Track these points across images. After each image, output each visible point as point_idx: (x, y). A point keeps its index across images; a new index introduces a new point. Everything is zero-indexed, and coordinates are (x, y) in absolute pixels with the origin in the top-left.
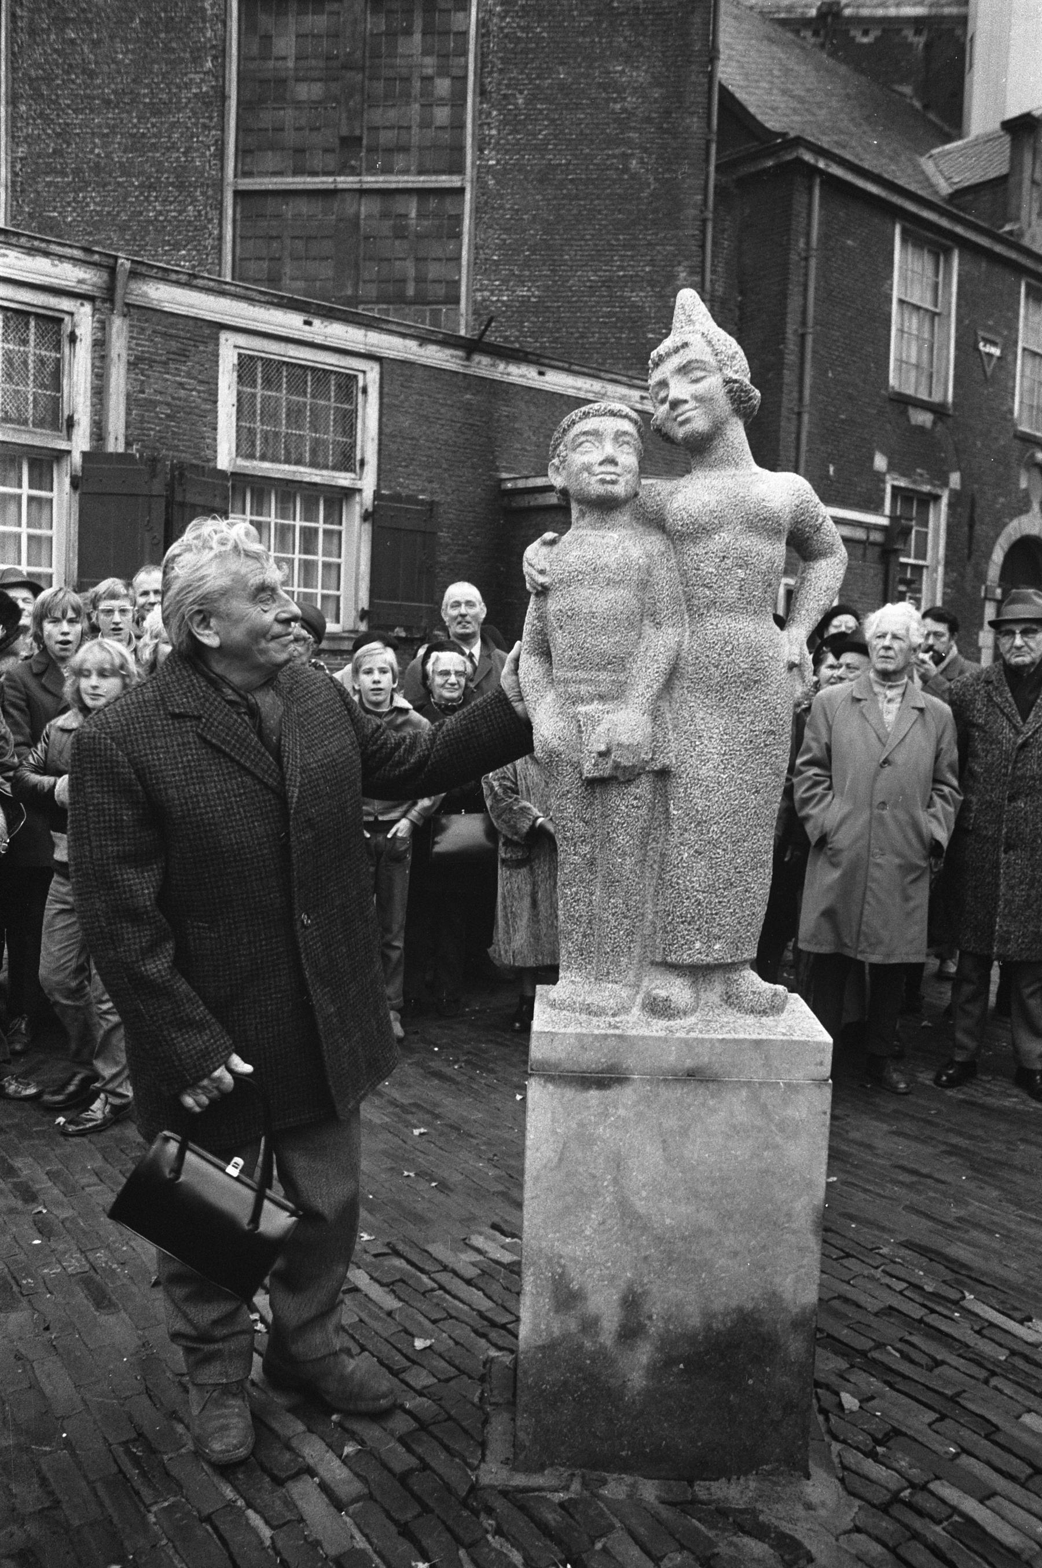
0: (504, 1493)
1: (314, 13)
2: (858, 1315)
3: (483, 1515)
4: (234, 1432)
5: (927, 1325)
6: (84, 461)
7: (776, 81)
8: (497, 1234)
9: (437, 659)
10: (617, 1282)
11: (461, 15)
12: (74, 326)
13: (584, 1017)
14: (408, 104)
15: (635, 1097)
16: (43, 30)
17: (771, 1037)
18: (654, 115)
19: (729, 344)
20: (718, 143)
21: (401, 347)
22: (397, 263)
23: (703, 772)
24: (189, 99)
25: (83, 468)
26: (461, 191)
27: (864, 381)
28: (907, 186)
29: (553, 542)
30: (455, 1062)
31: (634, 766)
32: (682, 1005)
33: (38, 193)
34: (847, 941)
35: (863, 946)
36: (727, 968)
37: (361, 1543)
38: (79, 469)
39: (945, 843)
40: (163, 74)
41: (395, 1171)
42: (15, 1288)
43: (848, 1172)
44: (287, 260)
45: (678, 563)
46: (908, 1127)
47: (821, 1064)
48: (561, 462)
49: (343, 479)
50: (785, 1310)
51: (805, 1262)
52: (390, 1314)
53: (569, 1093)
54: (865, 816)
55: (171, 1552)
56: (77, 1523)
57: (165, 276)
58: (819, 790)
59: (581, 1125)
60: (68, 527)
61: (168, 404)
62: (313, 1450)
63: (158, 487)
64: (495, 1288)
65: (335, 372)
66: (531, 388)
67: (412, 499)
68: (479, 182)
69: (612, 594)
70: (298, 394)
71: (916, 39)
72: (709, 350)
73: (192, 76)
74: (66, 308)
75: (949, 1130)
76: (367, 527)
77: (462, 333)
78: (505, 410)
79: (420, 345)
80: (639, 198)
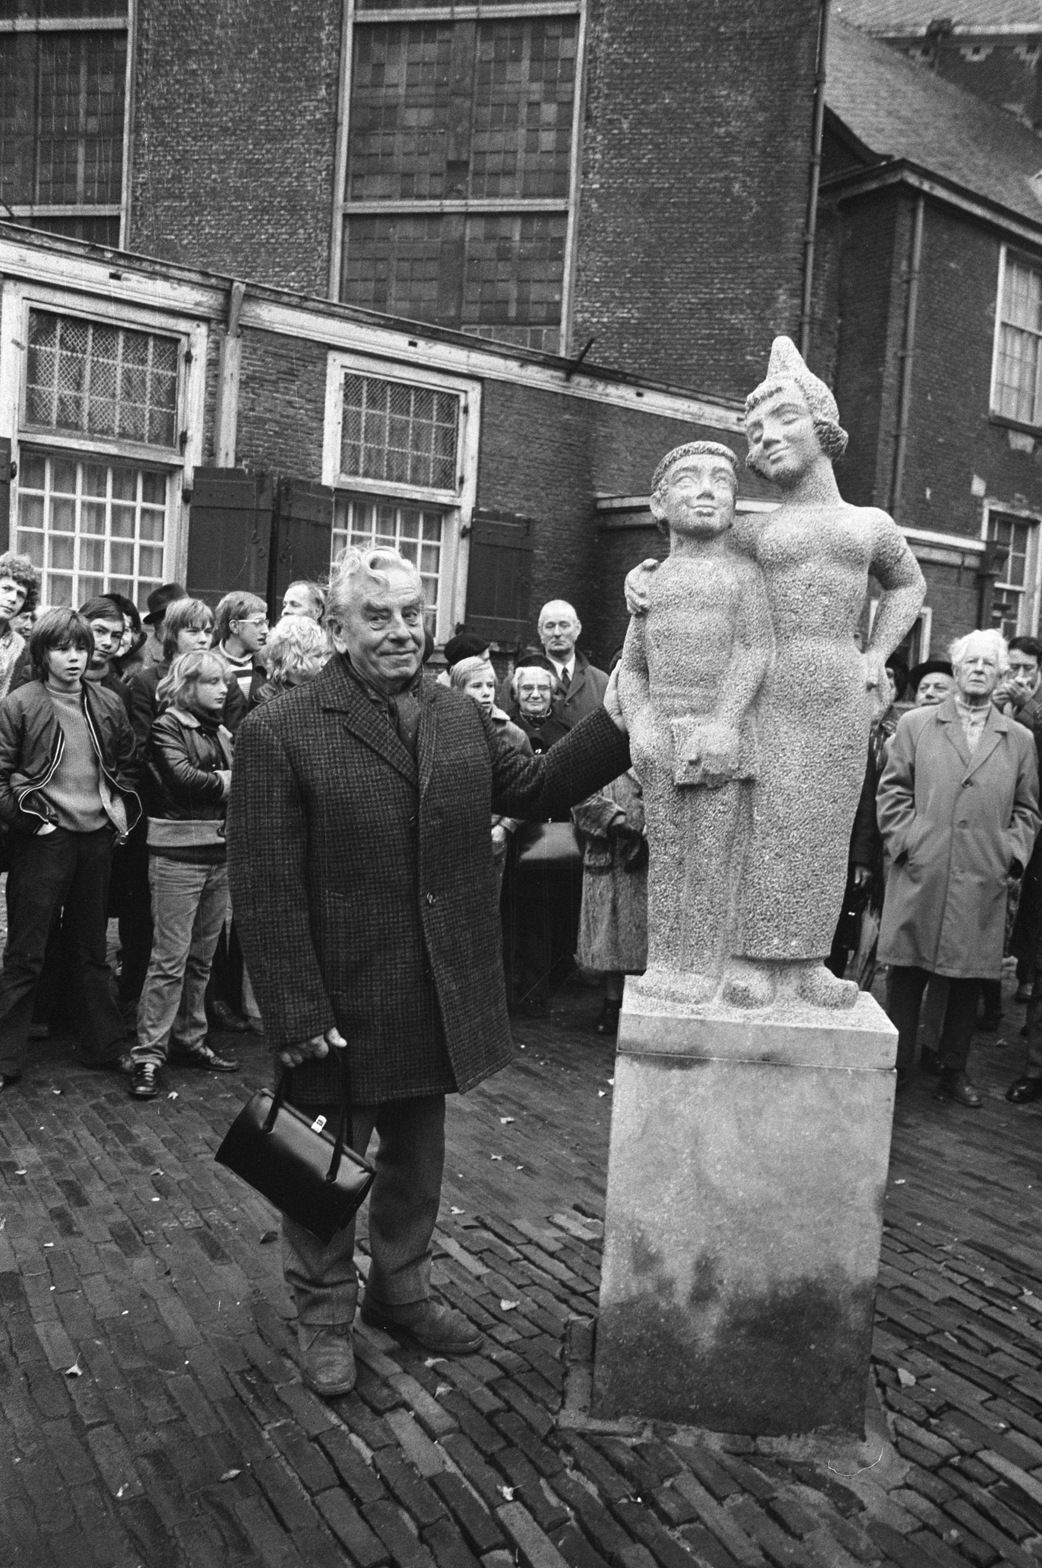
0: (582, 1435)
1: (426, 41)
2: (918, 1304)
3: (561, 1452)
4: (338, 1368)
5: (985, 1316)
6: (195, 476)
7: (882, 102)
8: (580, 1215)
9: (522, 674)
10: (691, 1248)
11: (568, 42)
12: (190, 345)
13: (669, 1003)
14: (515, 129)
15: (714, 1078)
16: (167, 62)
17: (842, 1028)
18: (758, 139)
19: (821, 389)
20: (822, 168)
21: (502, 368)
22: (501, 284)
23: (785, 781)
24: (303, 126)
25: (195, 482)
26: (565, 214)
27: (964, 405)
28: (1013, 208)
29: (652, 569)
30: (542, 1059)
31: (722, 774)
32: (759, 996)
33: (157, 217)
34: (925, 955)
35: (941, 960)
36: (802, 963)
37: (451, 1467)
38: (191, 482)
39: (1025, 863)
40: (279, 102)
41: (484, 1155)
42: (138, 1238)
43: (917, 1176)
44: (394, 283)
45: (767, 589)
46: (976, 1137)
47: (887, 1054)
48: (663, 495)
49: (443, 496)
50: (847, 1281)
51: (867, 1237)
52: (478, 1278)
53: (653, 1071)
54: (946, 833)
55: (284, 1463)
56: (201, 1434)
57: (277, 298)
58: (902, 808)
59: (664, 1101)
60: (179, 538)
61: (277, 422)
62: (409, 1388)
63: (265, 502)
64: (576, 1262)
65: (438, 392)
66: (628, 409)
67: (509, 517)
68: (583, 205)
69: (705, 617)
70: (401, 413)
71: (1028, 57)
72: (801, 394)
73: (306, 104)
74: (183, 330)
75: (1016, 1143)
76: (465, 543)
77: (562, 354)
78: (603, 431)
79: (521, 366)
80: (741, 221)
